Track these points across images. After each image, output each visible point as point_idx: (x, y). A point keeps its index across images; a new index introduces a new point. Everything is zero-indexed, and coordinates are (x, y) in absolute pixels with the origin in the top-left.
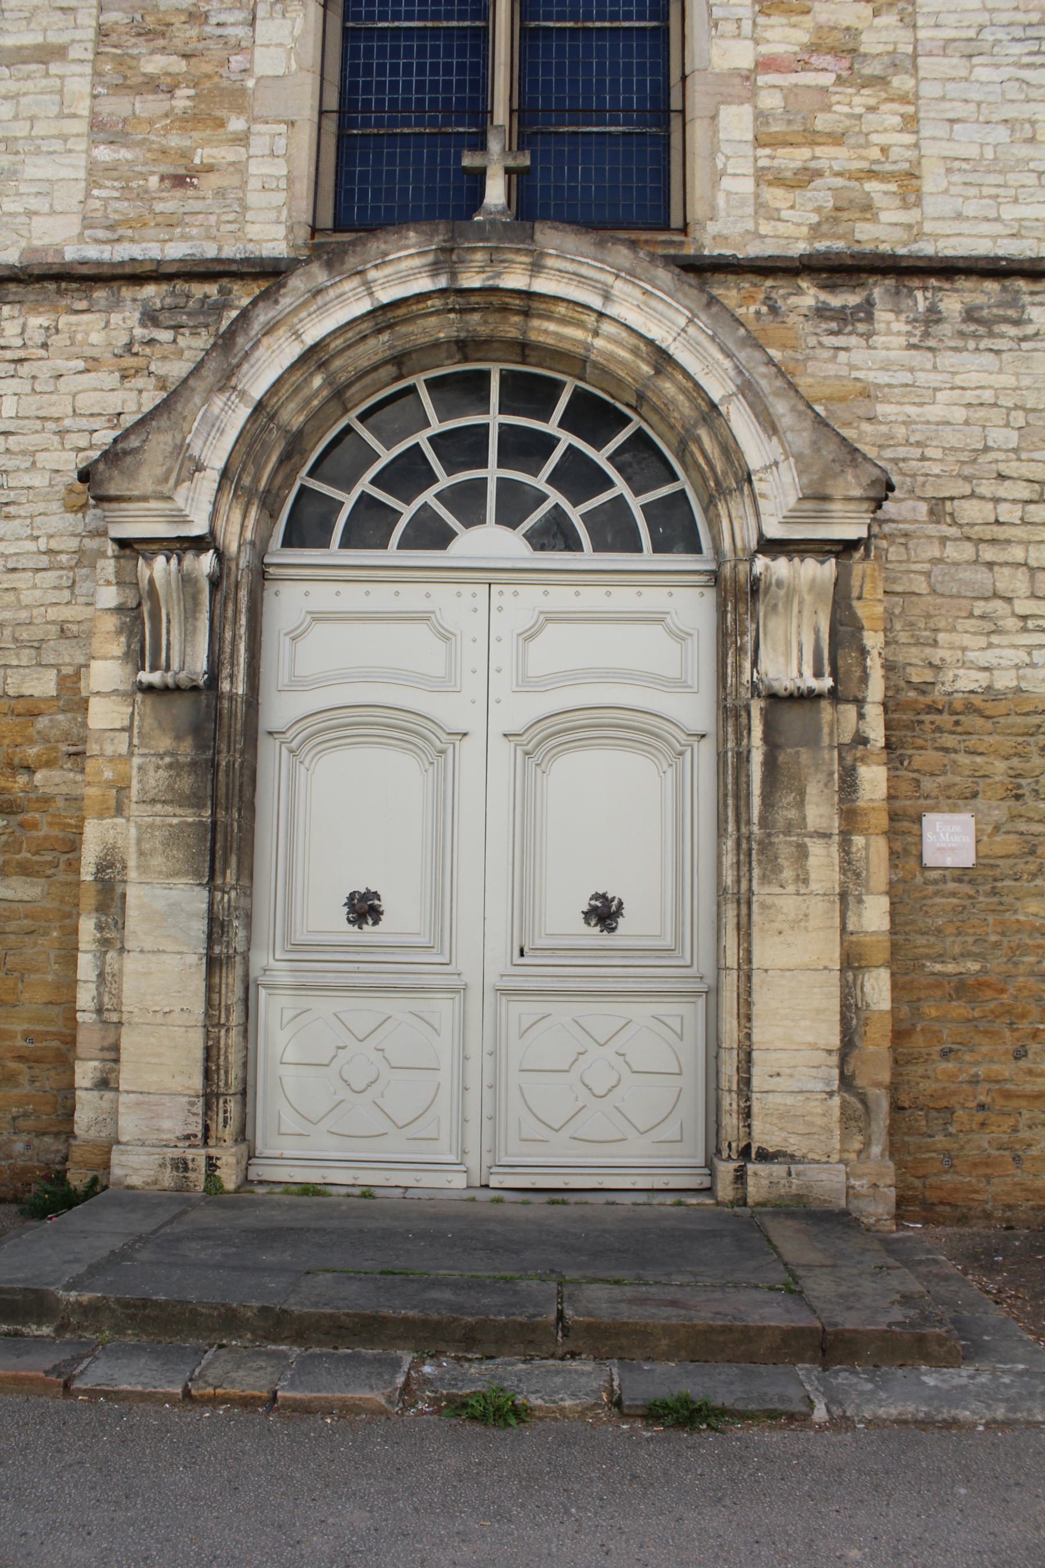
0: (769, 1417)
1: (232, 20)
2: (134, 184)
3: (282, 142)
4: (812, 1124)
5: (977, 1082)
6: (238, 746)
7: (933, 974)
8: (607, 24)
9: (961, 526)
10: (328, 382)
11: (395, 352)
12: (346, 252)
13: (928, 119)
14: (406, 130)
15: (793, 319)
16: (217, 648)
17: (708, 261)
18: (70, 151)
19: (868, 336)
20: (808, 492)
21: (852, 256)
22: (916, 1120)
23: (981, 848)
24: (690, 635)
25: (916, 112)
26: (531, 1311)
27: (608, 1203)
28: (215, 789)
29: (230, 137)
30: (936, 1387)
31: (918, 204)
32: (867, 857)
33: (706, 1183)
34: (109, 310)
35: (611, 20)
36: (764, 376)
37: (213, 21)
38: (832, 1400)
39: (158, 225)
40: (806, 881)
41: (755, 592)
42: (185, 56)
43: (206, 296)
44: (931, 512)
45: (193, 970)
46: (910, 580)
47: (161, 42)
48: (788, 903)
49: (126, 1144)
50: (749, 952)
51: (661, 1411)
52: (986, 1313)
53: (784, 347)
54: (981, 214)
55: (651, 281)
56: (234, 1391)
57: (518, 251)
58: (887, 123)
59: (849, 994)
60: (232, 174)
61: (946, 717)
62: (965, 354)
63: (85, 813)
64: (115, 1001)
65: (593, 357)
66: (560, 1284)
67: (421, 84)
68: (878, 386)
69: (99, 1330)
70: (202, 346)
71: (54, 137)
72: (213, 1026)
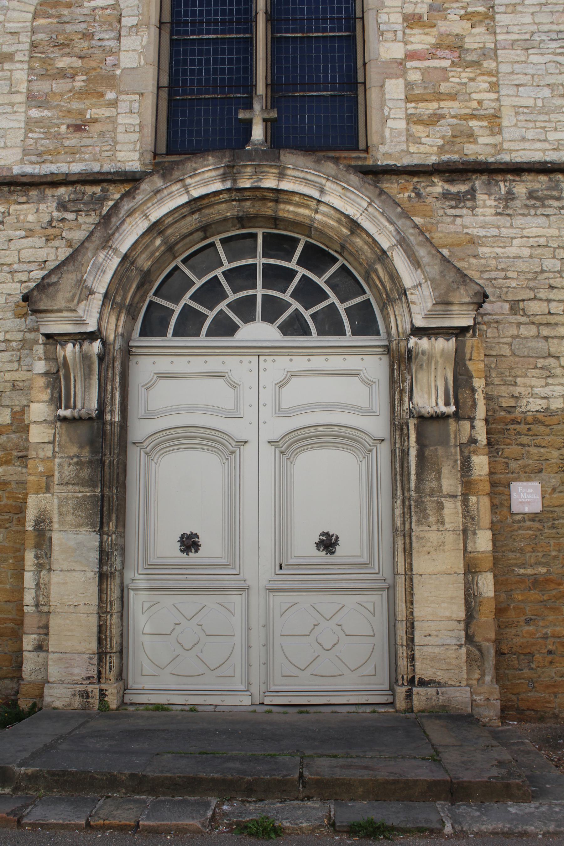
0: (419, 831)
1: (107, 37)
2: (52, 130)
3: (137, 105)
4: (450, 664)
5: (547, 638)
6: (116, 451)
7: (520, 575)
8: (321, 34)
9: (529, 316)
10: (164, 242)
11: (202, 224)
12: (173, 169)
13: (504, 84)
14: (207, 96)
15: (429, 200)
16: (103, 395)
17: (380, 168)
18: (16, 112)
19: (473, 208)
20: (439, 300)
21: (462, 164)
22: (512, 661)
23: (545, 501)
24: (374, 382)
25: (497, 81)
26: (285, 773)
27: (333, 712)
28: (102, 476)
29: (107, 102)
30: (516, 813)
31: (500, 133)
32: (478, 508)
33: (391, 700)
34: (38, 202)
35: (323, 32)
36: (412, 234)
37: (97, 38)
38: (455, 821)
39: (66, 153)
40: (443, 523)
41: (410, 358)
42: (81, 57)
43: (94, 193)
44: (511, 309)
45: (91, 581)
46: (500, 348)
47: (67, 50)
48: (433, 536)
49: (53, 683)
50: (411, 564)
51: (357, 829)
52: (549, 772)
53: (425, 216)
54: (536, 137)
55: (346, 182)
56: (115, 822)
57: (271, 166)
58: (481, 88)
59: (470, 588)
60: (108, 123)
61: (522, 426)
62: (529, 217)
63: (28, 491)
64: (46, 599)
65: (315, 225)
66: (302, 758)
67: (215, 70)
68: (479, 237)
69: (38, 790)
70: (92, 222)
71: (6, 104)
72: (103, 613)
